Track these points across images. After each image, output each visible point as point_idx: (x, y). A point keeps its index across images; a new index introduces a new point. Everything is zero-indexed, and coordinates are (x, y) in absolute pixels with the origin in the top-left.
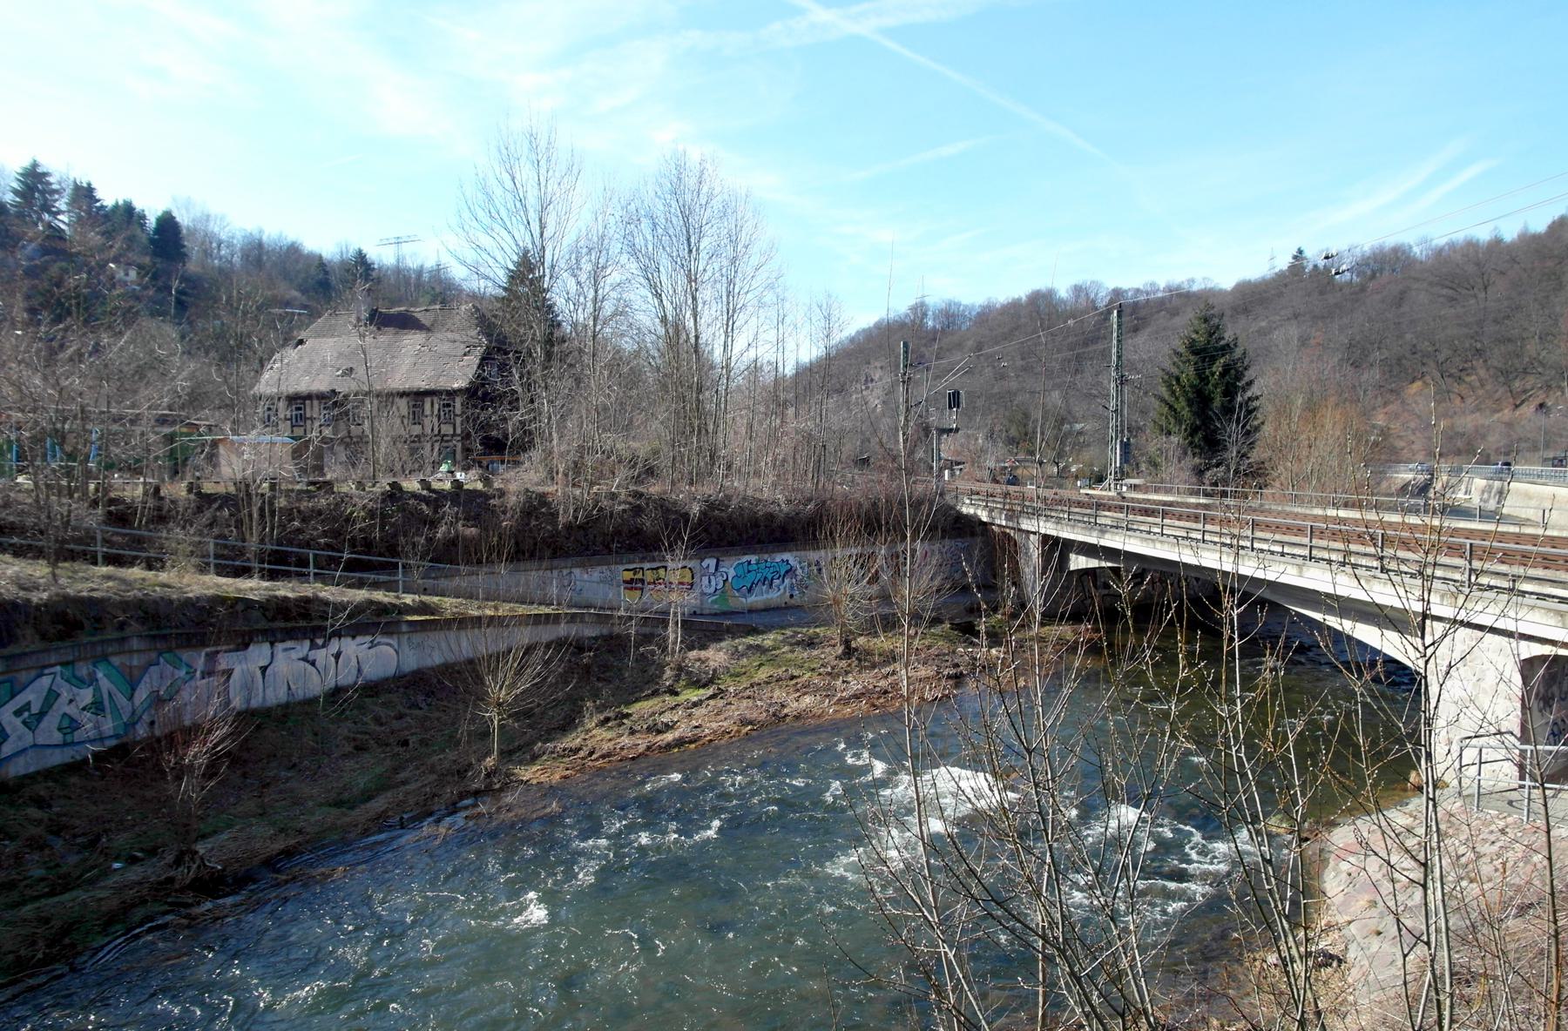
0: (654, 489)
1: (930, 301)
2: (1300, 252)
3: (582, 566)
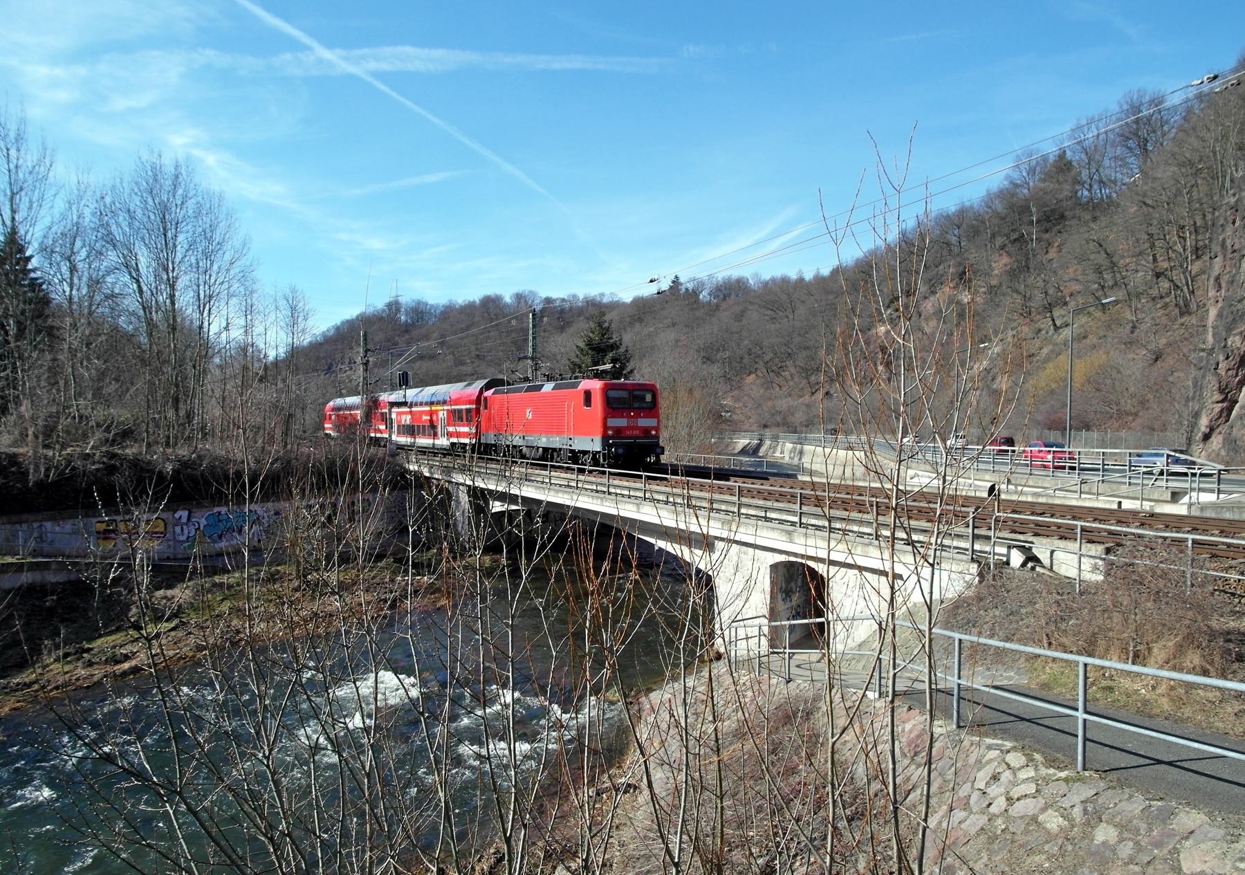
1: (402, 300)
2: (676, 277)
3: (53, 519)
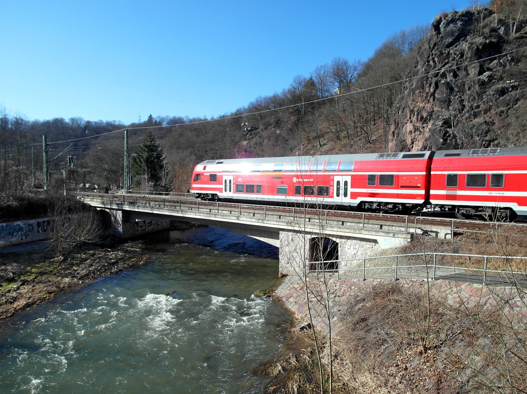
2: (151, 116)
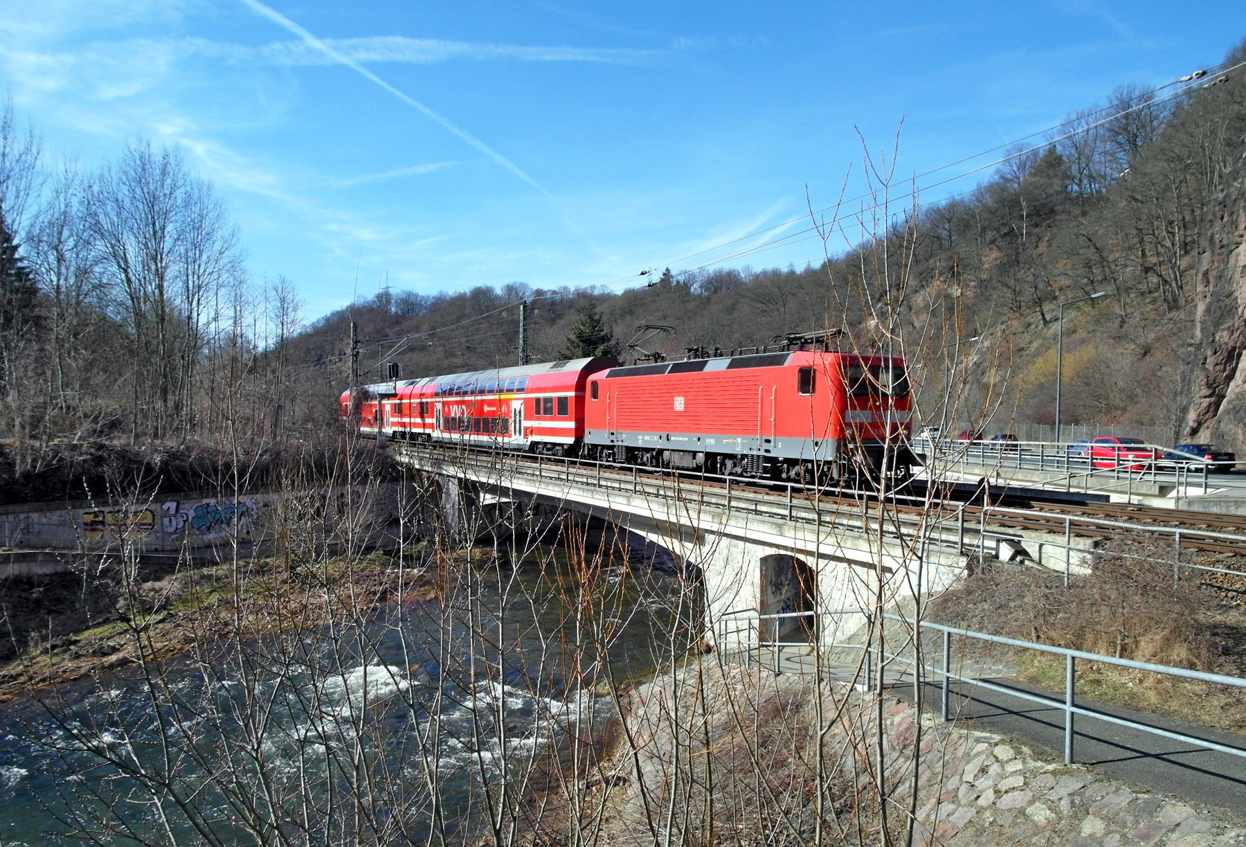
0: (118, 441)
1: (393, 291)
2: (667, 270)
3: (40, 510)
